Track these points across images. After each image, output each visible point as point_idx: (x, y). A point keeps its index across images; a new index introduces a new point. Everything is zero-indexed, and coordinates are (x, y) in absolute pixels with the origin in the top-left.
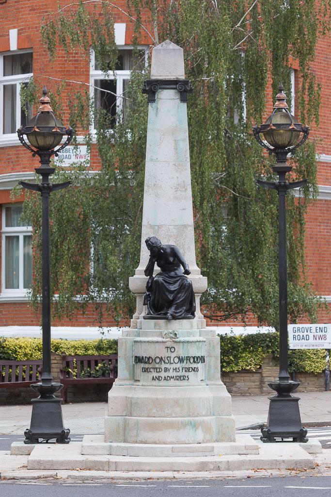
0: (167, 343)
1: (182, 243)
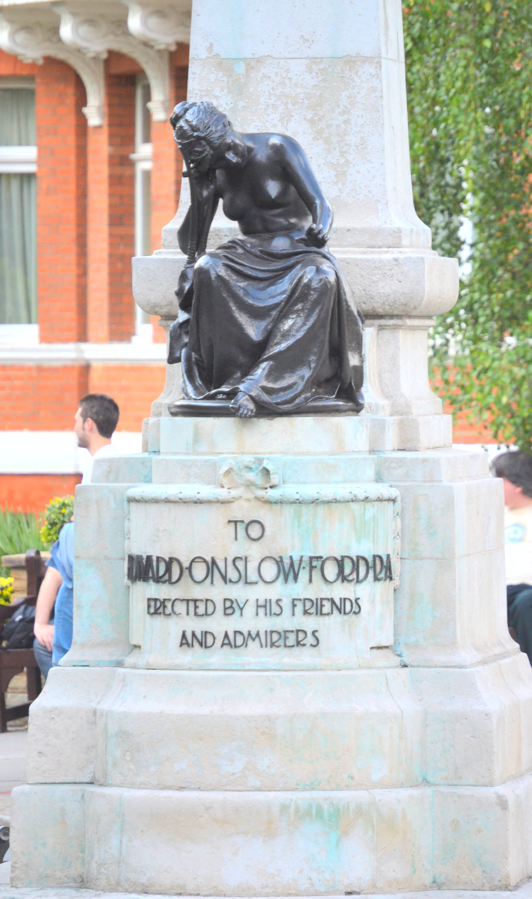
0: (234, 506)
1: (338, 126)
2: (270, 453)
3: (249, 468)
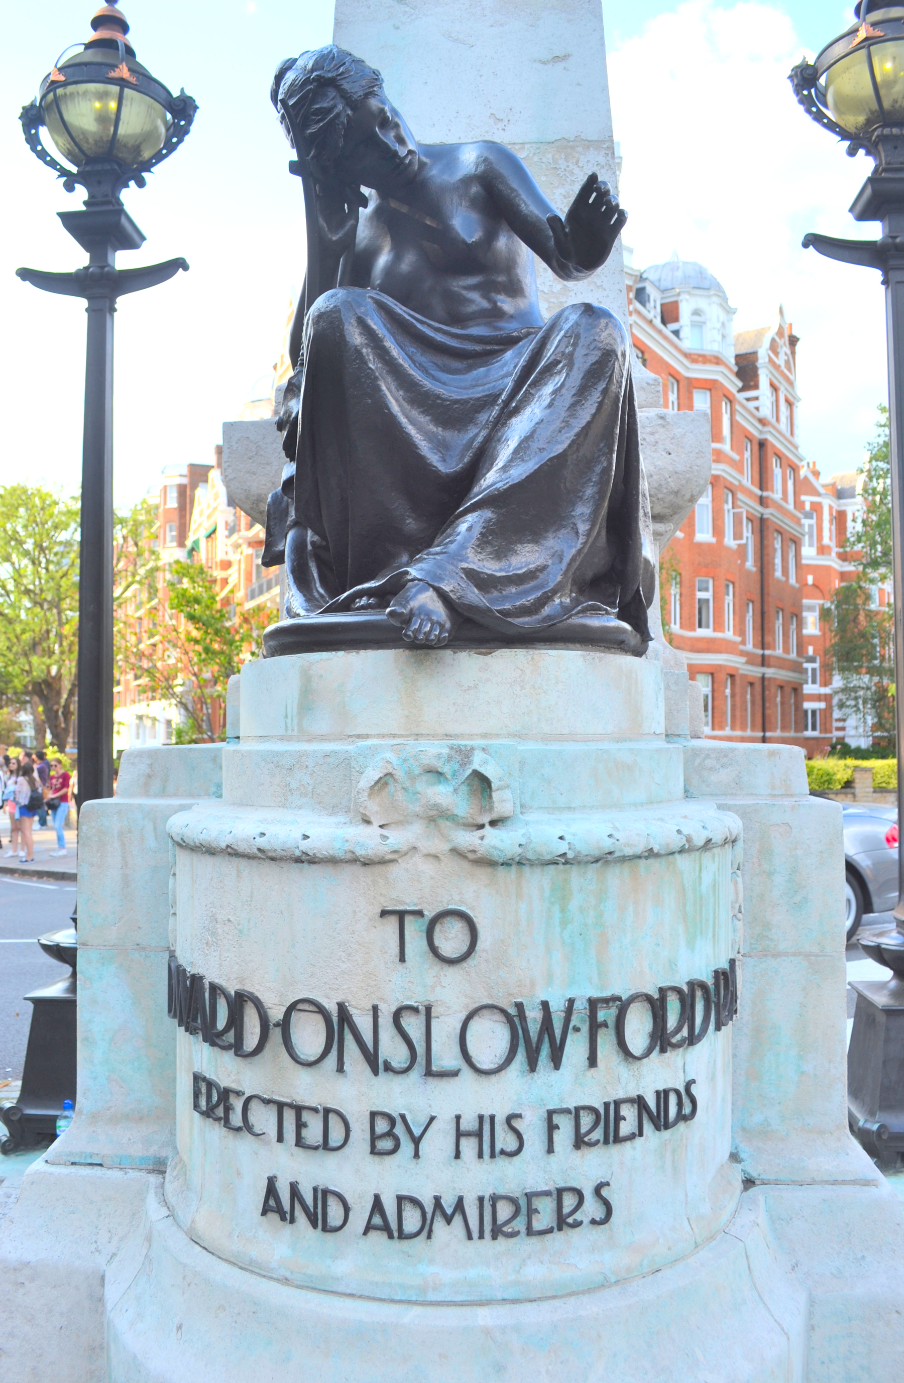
0: (395, 871)
2: (485, 736)
3: (436, 774)
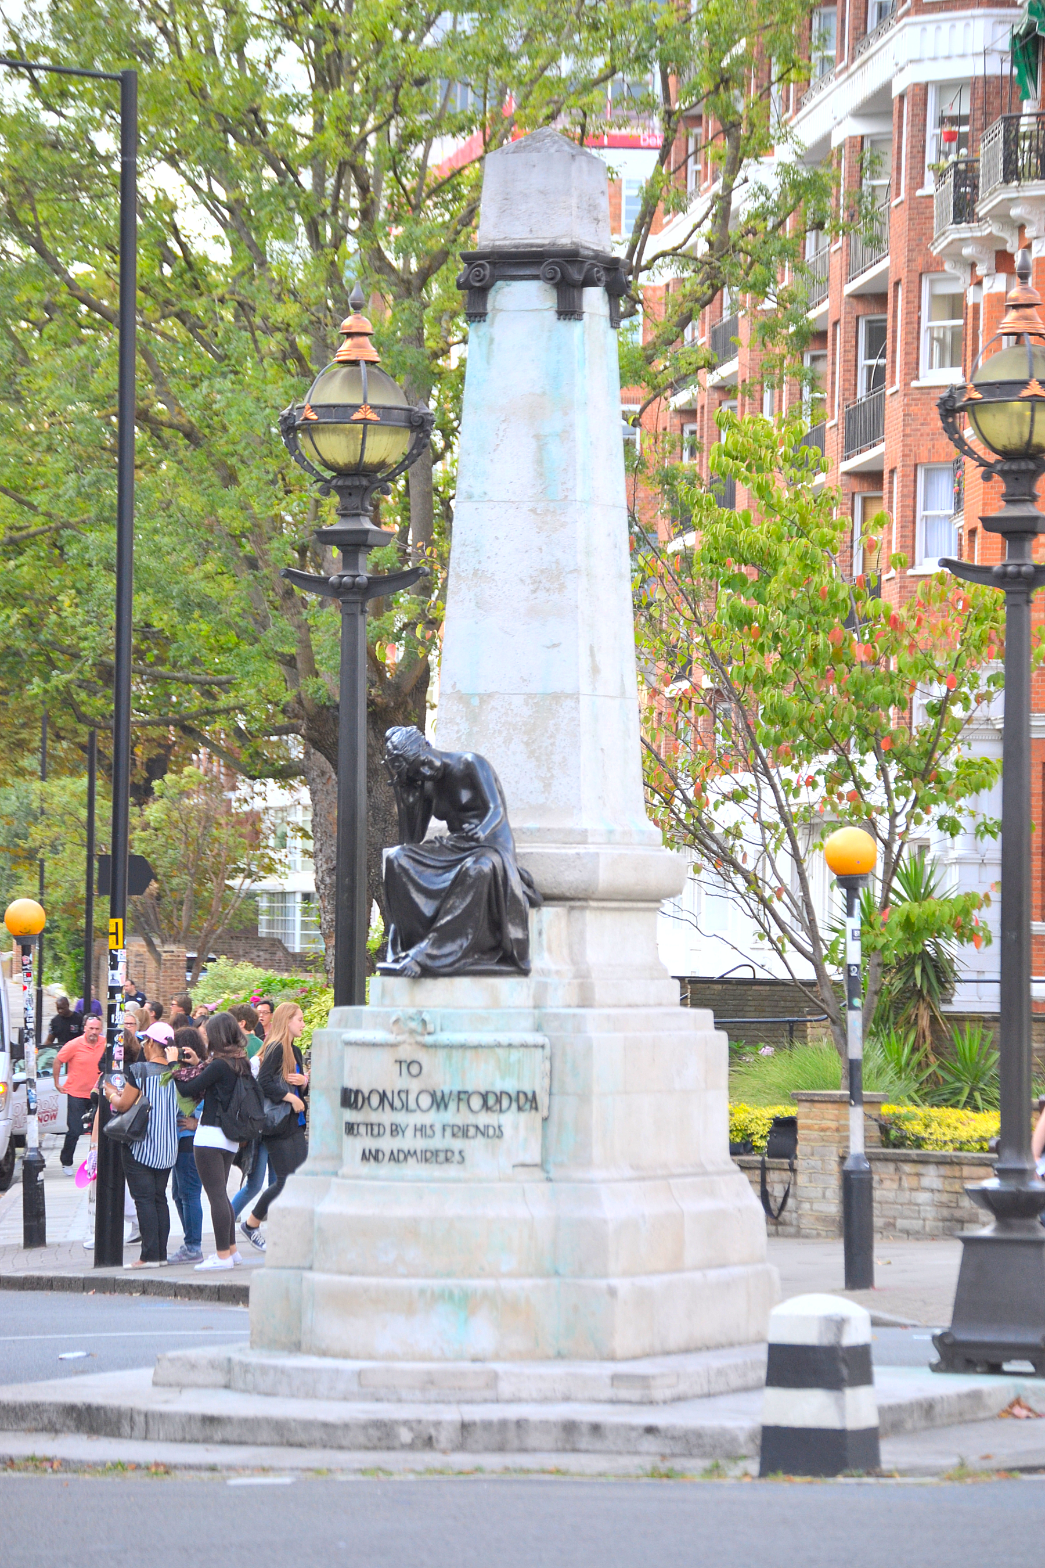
0: (401, 1049)
3: (411, 1019)
